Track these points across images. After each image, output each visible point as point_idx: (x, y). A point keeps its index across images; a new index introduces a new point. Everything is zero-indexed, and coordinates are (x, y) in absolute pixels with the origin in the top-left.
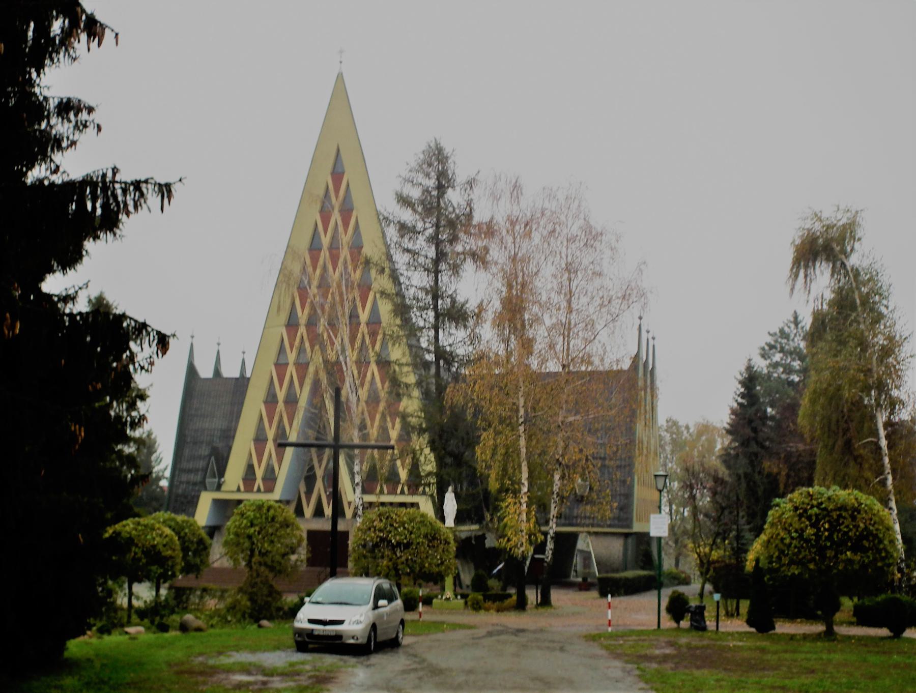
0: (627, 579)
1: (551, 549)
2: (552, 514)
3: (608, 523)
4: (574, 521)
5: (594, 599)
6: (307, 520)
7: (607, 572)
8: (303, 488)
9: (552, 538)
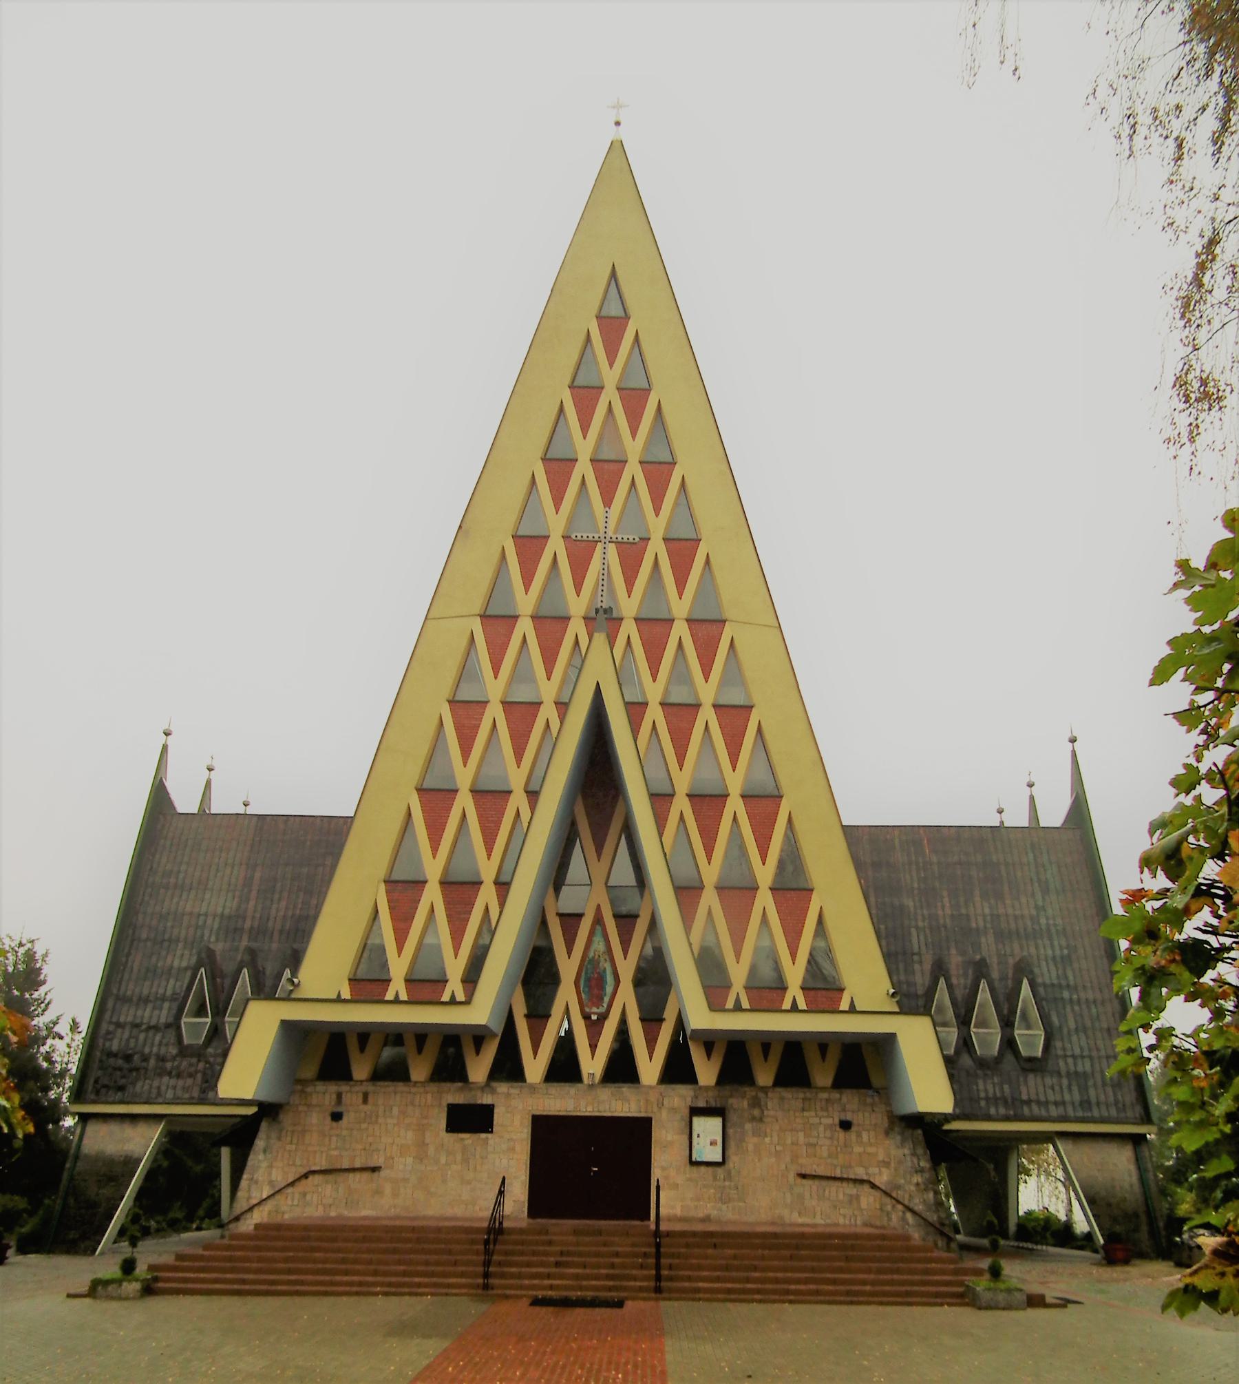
4: (1026, 1110)
6: (533, 1088)
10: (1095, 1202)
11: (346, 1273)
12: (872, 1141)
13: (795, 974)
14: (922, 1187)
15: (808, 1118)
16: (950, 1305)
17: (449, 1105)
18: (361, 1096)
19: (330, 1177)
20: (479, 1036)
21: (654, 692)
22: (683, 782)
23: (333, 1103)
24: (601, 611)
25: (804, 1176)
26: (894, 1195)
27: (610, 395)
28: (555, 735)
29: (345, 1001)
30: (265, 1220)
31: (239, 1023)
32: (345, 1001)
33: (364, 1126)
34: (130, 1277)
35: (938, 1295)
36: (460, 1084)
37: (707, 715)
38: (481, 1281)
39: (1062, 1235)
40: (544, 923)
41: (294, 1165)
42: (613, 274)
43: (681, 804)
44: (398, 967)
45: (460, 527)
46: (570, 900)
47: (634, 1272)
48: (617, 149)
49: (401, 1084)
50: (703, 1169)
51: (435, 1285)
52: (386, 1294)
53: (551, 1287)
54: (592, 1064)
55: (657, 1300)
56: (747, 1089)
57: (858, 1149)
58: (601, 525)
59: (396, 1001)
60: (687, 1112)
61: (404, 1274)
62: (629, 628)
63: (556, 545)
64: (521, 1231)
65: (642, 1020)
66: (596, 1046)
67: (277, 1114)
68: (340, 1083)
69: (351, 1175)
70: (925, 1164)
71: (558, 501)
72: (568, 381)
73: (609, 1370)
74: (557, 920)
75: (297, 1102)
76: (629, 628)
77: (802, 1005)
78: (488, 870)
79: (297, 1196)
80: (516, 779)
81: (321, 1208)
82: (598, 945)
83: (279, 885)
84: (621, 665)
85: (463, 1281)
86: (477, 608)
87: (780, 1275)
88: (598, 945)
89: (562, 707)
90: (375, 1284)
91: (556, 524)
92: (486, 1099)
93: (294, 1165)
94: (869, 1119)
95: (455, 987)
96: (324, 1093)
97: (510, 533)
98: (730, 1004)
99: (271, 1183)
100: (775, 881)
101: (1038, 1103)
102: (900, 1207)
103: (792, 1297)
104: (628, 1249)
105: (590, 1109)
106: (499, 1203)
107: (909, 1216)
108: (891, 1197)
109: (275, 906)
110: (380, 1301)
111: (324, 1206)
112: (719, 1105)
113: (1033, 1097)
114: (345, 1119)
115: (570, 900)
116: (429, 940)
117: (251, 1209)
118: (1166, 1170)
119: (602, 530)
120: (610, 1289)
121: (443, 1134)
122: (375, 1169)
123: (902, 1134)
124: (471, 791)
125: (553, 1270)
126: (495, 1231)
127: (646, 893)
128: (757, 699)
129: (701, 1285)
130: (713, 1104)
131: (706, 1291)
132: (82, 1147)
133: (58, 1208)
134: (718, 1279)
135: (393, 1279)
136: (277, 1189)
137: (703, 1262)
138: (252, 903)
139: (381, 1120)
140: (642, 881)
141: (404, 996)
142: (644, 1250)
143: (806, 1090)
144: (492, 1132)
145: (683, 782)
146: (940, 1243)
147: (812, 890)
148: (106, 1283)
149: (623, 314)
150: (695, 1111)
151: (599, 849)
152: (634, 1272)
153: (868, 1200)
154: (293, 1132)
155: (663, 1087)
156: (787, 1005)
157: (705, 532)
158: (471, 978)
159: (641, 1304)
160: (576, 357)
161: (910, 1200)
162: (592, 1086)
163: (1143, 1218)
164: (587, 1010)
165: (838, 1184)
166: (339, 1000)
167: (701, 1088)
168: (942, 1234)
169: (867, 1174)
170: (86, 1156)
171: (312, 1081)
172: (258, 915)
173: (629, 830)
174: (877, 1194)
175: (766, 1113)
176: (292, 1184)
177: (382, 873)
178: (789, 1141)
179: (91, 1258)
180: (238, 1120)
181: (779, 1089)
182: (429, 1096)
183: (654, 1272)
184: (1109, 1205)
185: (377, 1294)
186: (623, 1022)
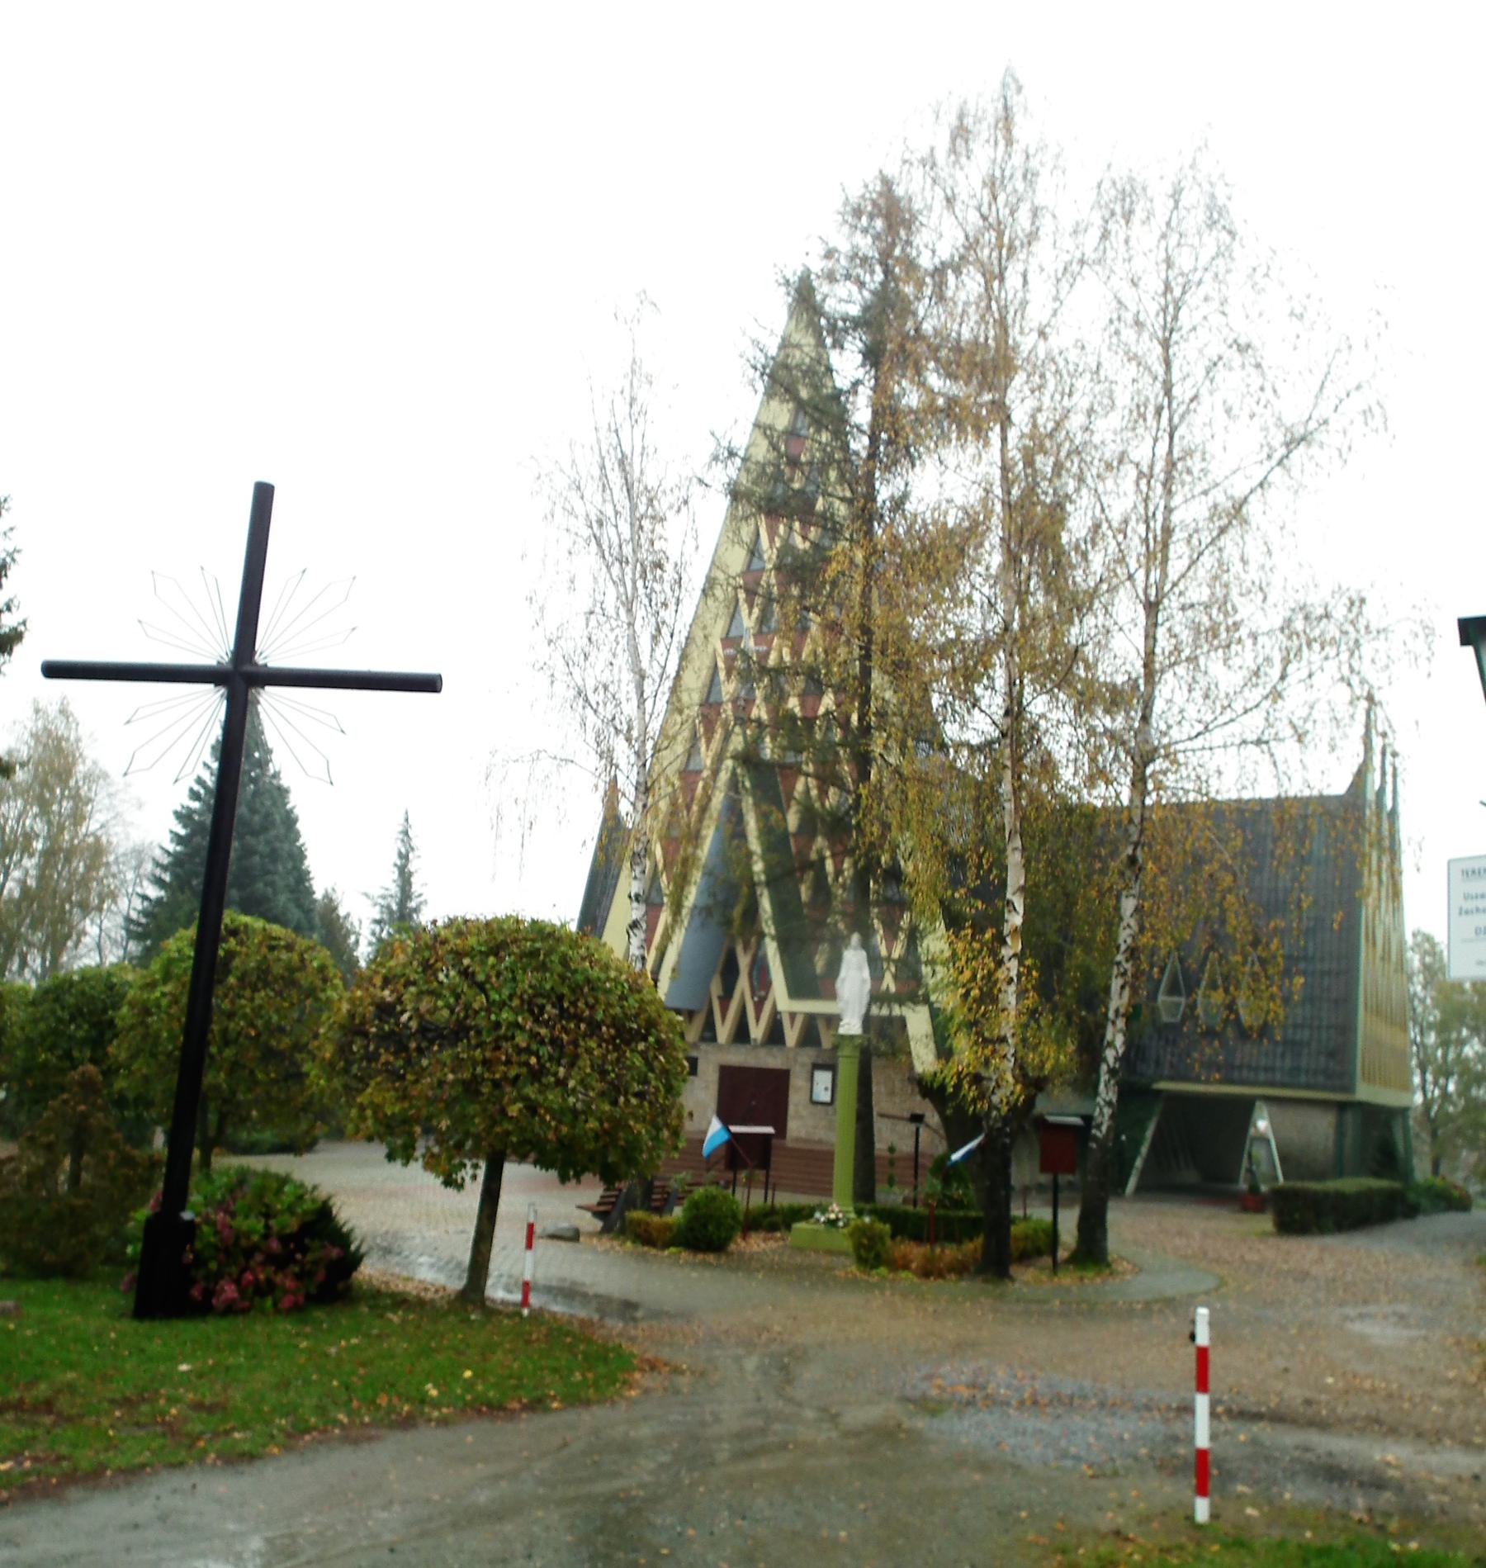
0: (1340, 1196)
1: (1109, 1104)
2: (1113, 1006)
3: (1303, 1079)
4: (1236, 1075)
5: (1264, 1235)
6: (721, 1047)
7: (1302, 1178)
8: (716, 989)
9: (1112, 1072)
54: (757, 1031)
60: (809, 1067)
101: (1250, 1068)
150: (817, 1066)
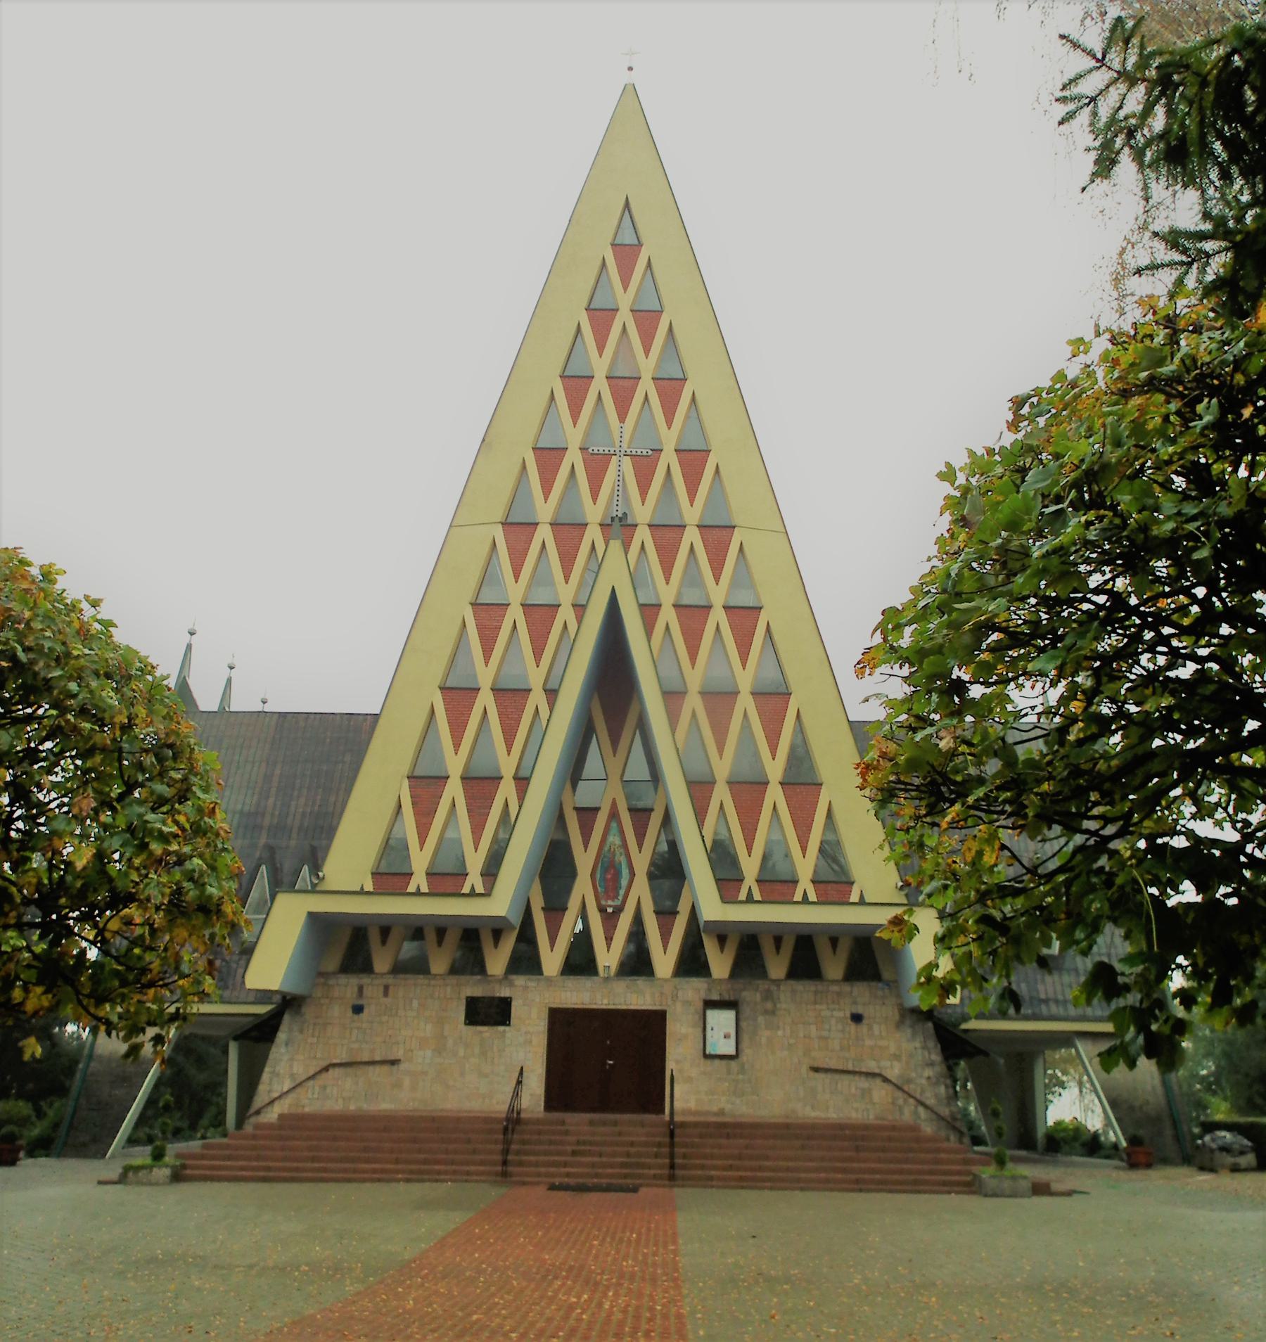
4: (1044, 1009)
5: (1117, 1168)
10: (1118, 1104)
11: (367, 1161)
12: (884, 1034)
13: (805, 866)
14: (934, 1080)
15: (821, 1010)
16: (957, 1193)
17: (467, 998)
18: (381, 989)
19: (349, 1070)
20: (498, 929)
21: (667, 594)
22: (694, 679)
23: (355, 996)
24: (617, 520)
25: (816, 1070)
26: (906, 1088)
27: (624, 317)
28: (572, 637)
29: (368, 893)
30: (286, 1112)
31: (266, 919)
32: (368, 893)
33: (385, 1018)
34: (160, 1163)
35: (944, 1184)
36: (479, 977)
37: (718, 616)
38: (499, 1168)
39: (1092, 1146)
40: (561, 819)
41: (315, 1057)
42: (627, 205)
43: (693, 702)
44: (420, 861)
45: (484, 440)
46: (586, 794)
47: (648, 1160)
48: (630, 91)
49: (421, 976)
50: (717, 1062)
51: (455, 1172)
52: (408, 1181)
53: (568, 1175)
54: (608, 957)
55: (672, 1187)
56: (760, 982)
57: (868, 1042)
58: (617, 439)
59: (418, 893)
60: (700, 1005)
61: (425, 1162)
62: (643, 535)
63: (574, 457)
64: (538, 1122)
65: (657, 913)
66: (611, 939)
67: (300, 1006)
68: (361, 976)
69: (371, 1068)
70: (936, 1057)
71: (575, 416)
72: (585, 304)
73: (623, 1232)
74: (574, 814)
75: (319, 995)
76: (643, 535)
77: (812, 897)
78: (508, 766)
79: (317, 1089)
80: (536, 678)
81: (340, 1101)
82: (614, 839)
83: (298, 781)
84: (636, 568)
85: (482, 1168)
86: (499, 516)
87: (791, 1164)
88: (614, 839)
89: (580, 609)
90: (397, 1172)
91: (573, 436)
92: (504, 992)
93: (315, 1057)
94: (879, 1010)
95: (475, 880)
96: (346, 986)
97: (530, 446)
98: (743, 896)
99: (292, 1076)
100: (784, 776)
101: (1057, 1002)
102: (911, 1101)
103: (802, 1185)
104: (643, 1139)
105: (605, 1001)
106: (516, 1094)
107: (921, 1110)
108: (904, 1091)
109: (293, 803)
110: (401, 1186)
111: (344, 1099)
112: (732, 998)
113: (1051, 995)
114: (366, 1011)
115: (586, 794)
116: (450, 834)
117: (272, 1102)
118: (1203, 1079)
119: (618, 444)
120: (626, 1176)
121: (462, 1026)
122: (394, 1062)
123: (912, 1027)
124: (492, 689)
125: (569, 1159)
126: (513, 1122)
127: (660, 789)
128: (765, 601)
129: (713, 1173)
130: (726, 997)
131: (719, 1178)
132: (96, 1047)
133: (70, 1110)
134: (731, 1167)
135: (414, 1167)
136: (297, 1082)
137: (716, 1151)
138: (271, 800)
139: (401, 1012)
140: (656, 777)
141: (425, 889)
142: (658, 1139)
143: (818, 983)
144: (509, 1025)
145: (694, 679)
146: (952, 1138)
147: (821, 784)
148: (137, 1169)
149: (636, 242)
150: (710, 1004)
151: (615, 740)
152: (648, 1160)
153: (880, 1093)
154: (315, 1024)
155: (677, 980)
156: (798, 897)
157: (715, 443)
158: (491, 871)
159: (655, 1190)
160: (592, 282)
161: (921, 1095)
162: (607, 979)
163: (1167, 1124)
164: (603, 902)
165: (851, 1077)
166: (362, 892)
167: (714, 981)
168: (954, 1128)
169: (879, 1067)
170: (100, 1056)
171: (334, 973)
172: (277, 813)
173: (643, 726)
174: (889, 1088)
175: (778, 1006)
176: (312, 1077)
177: (405, 769)
178: (801, 1035)
179: (102, 1161)
180: (251, 1019)
181: (792, 982)
182: (449, 989)
183: (667, 1161)
184: (1132, 1108)
185: (398, 1181)
186: (638, 920)
